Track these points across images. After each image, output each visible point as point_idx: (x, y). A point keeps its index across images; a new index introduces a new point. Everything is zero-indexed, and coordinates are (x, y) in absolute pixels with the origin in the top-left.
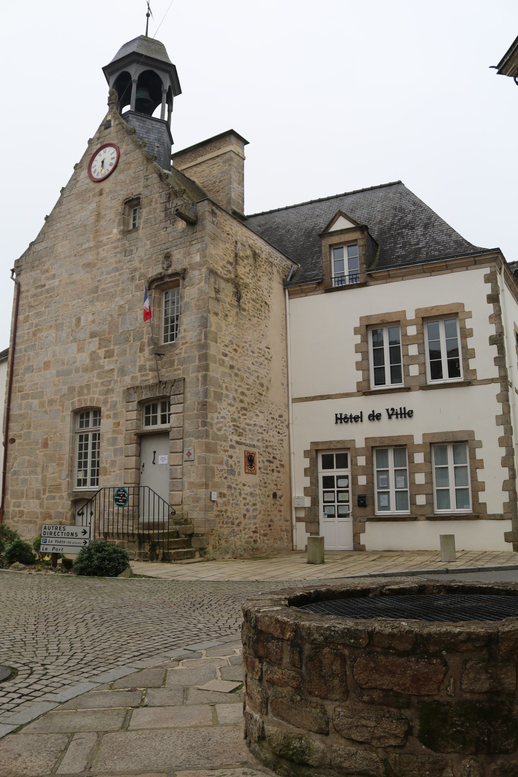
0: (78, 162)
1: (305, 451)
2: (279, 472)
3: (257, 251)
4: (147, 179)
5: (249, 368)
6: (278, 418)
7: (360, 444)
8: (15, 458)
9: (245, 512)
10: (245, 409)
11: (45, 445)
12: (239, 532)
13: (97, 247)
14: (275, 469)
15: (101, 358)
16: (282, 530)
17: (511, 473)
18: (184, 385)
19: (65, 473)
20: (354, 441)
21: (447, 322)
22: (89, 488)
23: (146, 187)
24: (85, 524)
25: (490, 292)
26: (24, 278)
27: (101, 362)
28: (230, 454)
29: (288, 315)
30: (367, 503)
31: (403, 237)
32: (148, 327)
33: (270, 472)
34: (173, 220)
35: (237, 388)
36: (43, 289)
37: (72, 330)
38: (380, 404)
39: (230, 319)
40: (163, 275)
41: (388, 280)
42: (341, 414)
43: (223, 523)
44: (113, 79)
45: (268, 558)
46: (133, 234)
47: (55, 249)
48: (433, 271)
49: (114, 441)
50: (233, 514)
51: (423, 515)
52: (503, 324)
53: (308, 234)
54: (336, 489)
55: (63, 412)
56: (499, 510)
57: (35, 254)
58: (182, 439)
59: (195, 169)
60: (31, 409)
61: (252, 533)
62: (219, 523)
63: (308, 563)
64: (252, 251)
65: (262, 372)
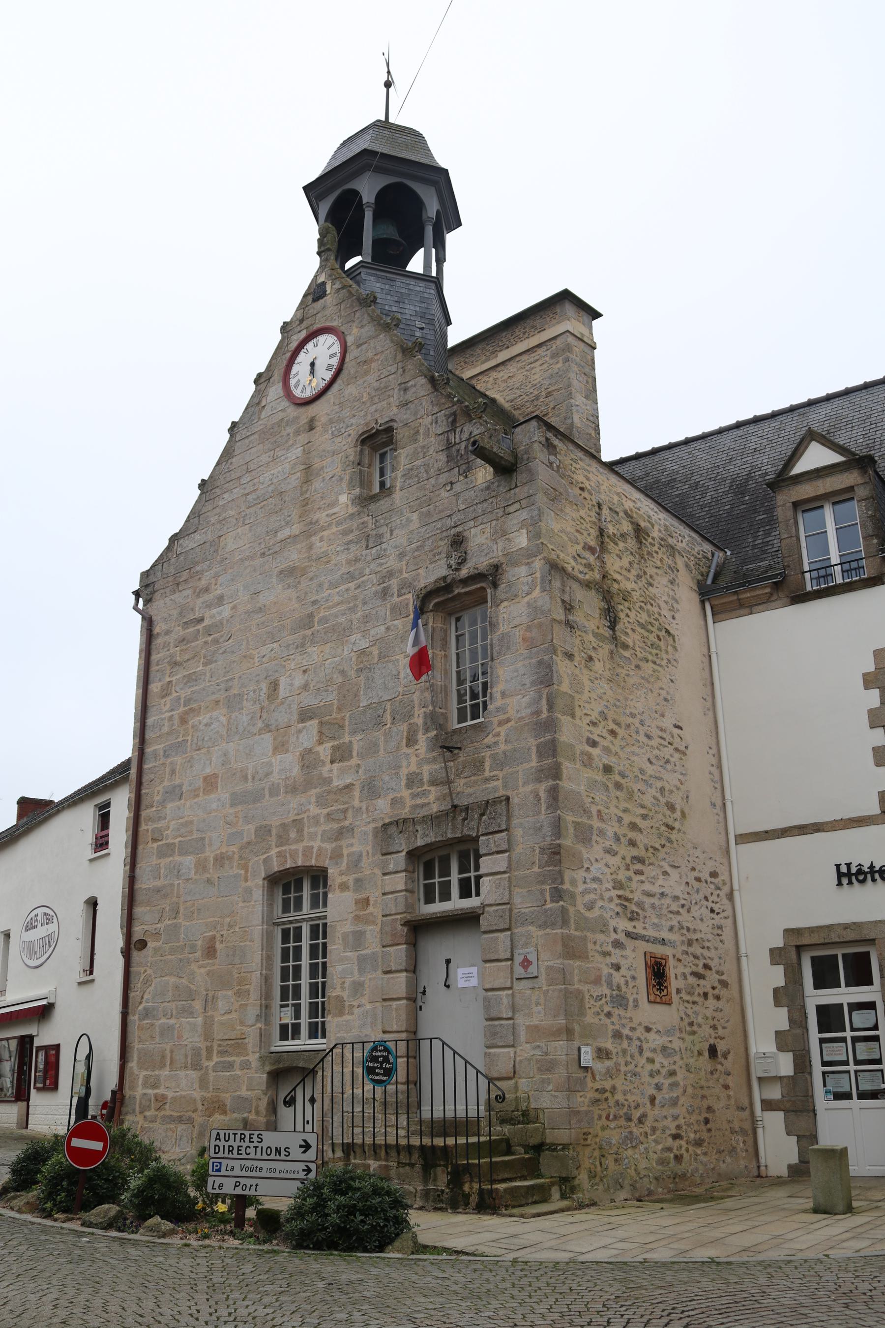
0: (262, 370)
1: (772, 951)
2: (718, 998)
3: (643, 524)
4: (405, 390)
5: (642, 771)
6: (709, 880)
8: (147, 982)
9: (654, 1092)
10: (641, 861)
11: (210, 952)
12: (642, 1139)
13: (308, 534)
14: (711, 992)
15: (323, 762)
16: (733, 1131)
18: (508, 811)
19: (253, 1011)
22: (304, 1043)
23: (405, 404)
24: (299, 1127)
26: (160, 608)
27: (325, 770)
28: (614, 960)
29: (714, 657)
32: (422, 692)
33: (700, 1000)
34: (464, 467)
35: (621, 814)
36: (200, 627)
37: (262, 708)
39: (598, 666)
40: (449, 580)
42: (848, 865)
43: (608, 1118)
44: (325, 207)
45: (712, 1198)
46: (382, 502)
47: (222, 544)
49: (358, 939)
50: (629, 1097)
53: (740, 487)
55: (246, 880)
57: (182, 558)
58: (509, 929)
59: (494, 374)
60: (178, 876)
61: (670, 1139)
62: (600, 1117)
63: (816, 1211)
64: (632, 523)
65: (671, 779)
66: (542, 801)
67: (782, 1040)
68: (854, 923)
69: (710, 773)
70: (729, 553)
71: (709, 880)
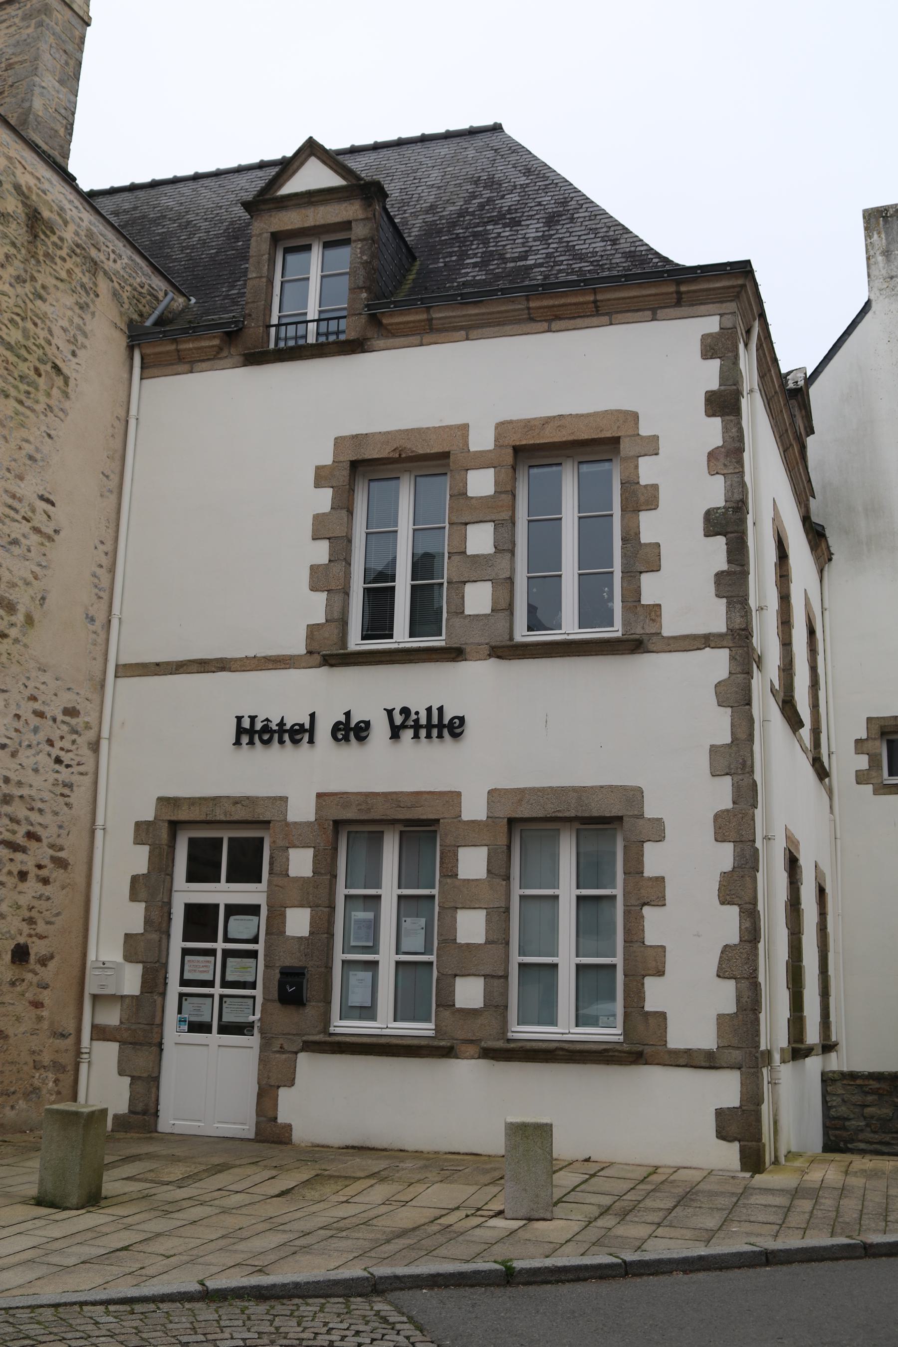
1: (138, 825)
2: (45, 881)
3: (46, 214)
6: (60, 717)
7: (301, 810)
16: (37, 1066)
17: (747, 924)
20: (284, 800)
21: (585, 468)
25: (714, 385)
30: (306, 994)
31: (486, 243)
38: (369, 693)
41: (427, 338)
48: (558, 318)
51: (471, 1042)
52: (747, 479)
54: (220, 945)
56: (705, 1038)
63: (40, 1202)
67: (132, 947)
68: (248, 798)
69: (94, 575)
70: (193, 300)
71: (60, 717)
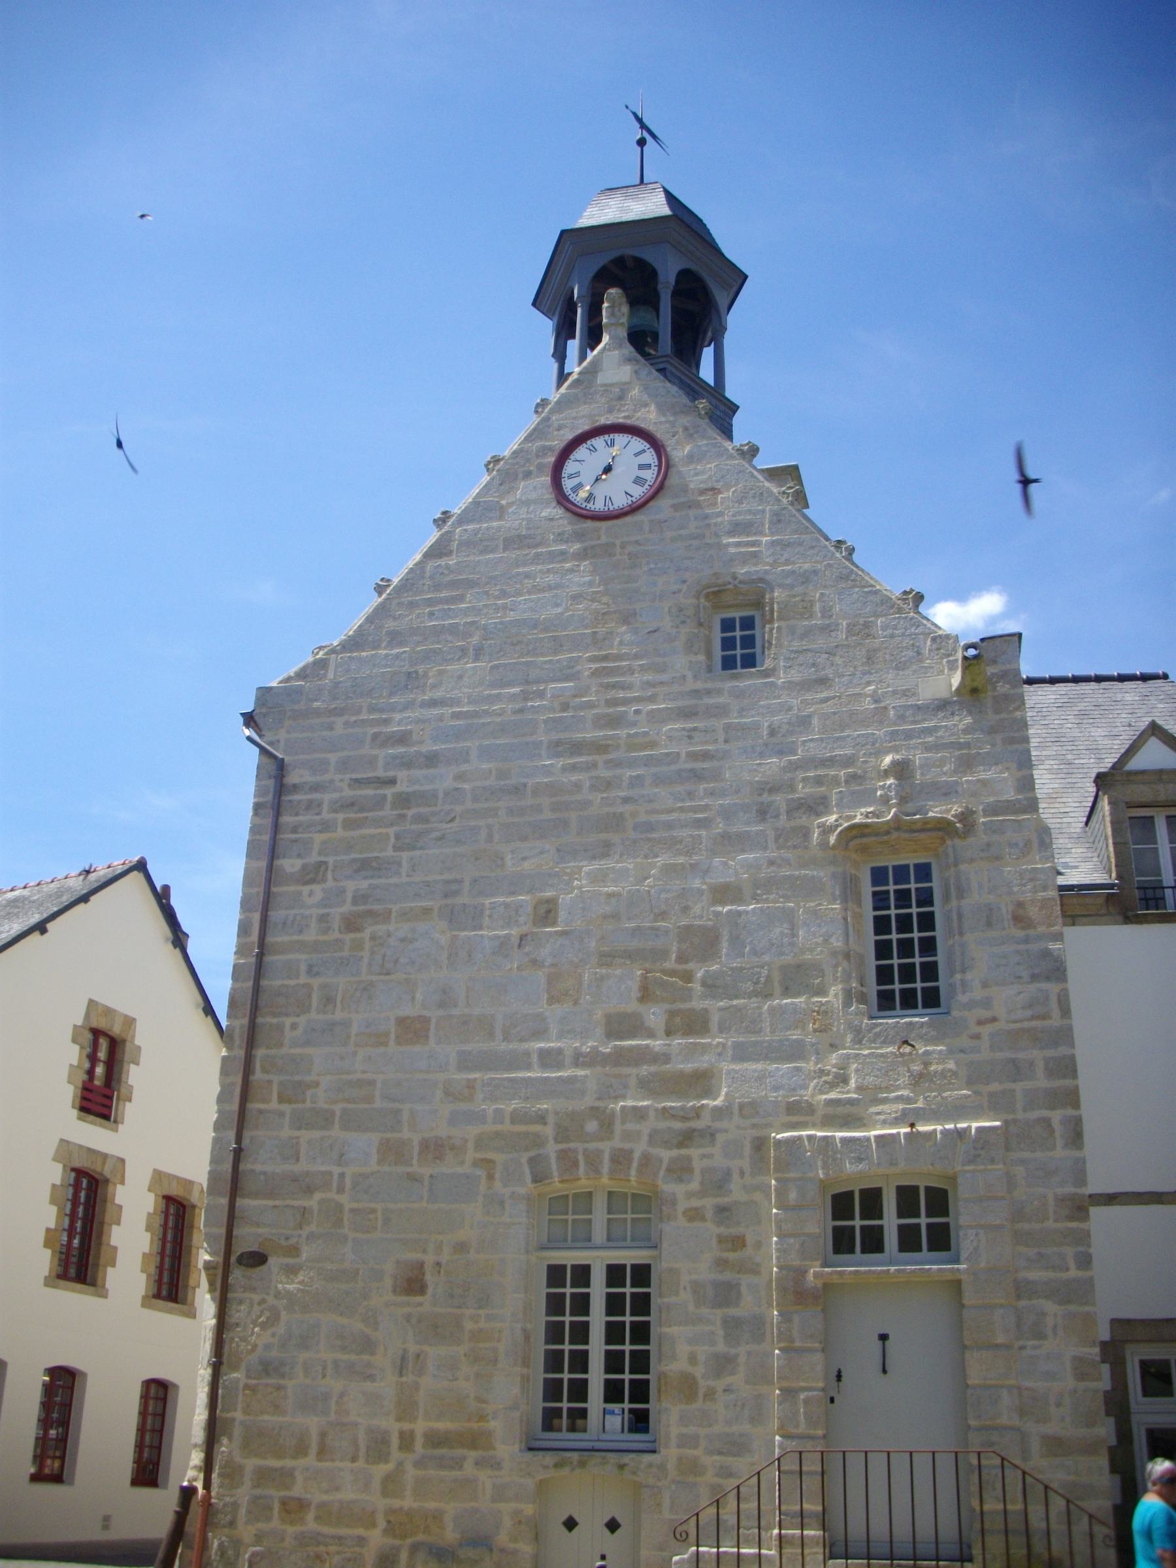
36: (389, 792)
66: (1057, 1134)
